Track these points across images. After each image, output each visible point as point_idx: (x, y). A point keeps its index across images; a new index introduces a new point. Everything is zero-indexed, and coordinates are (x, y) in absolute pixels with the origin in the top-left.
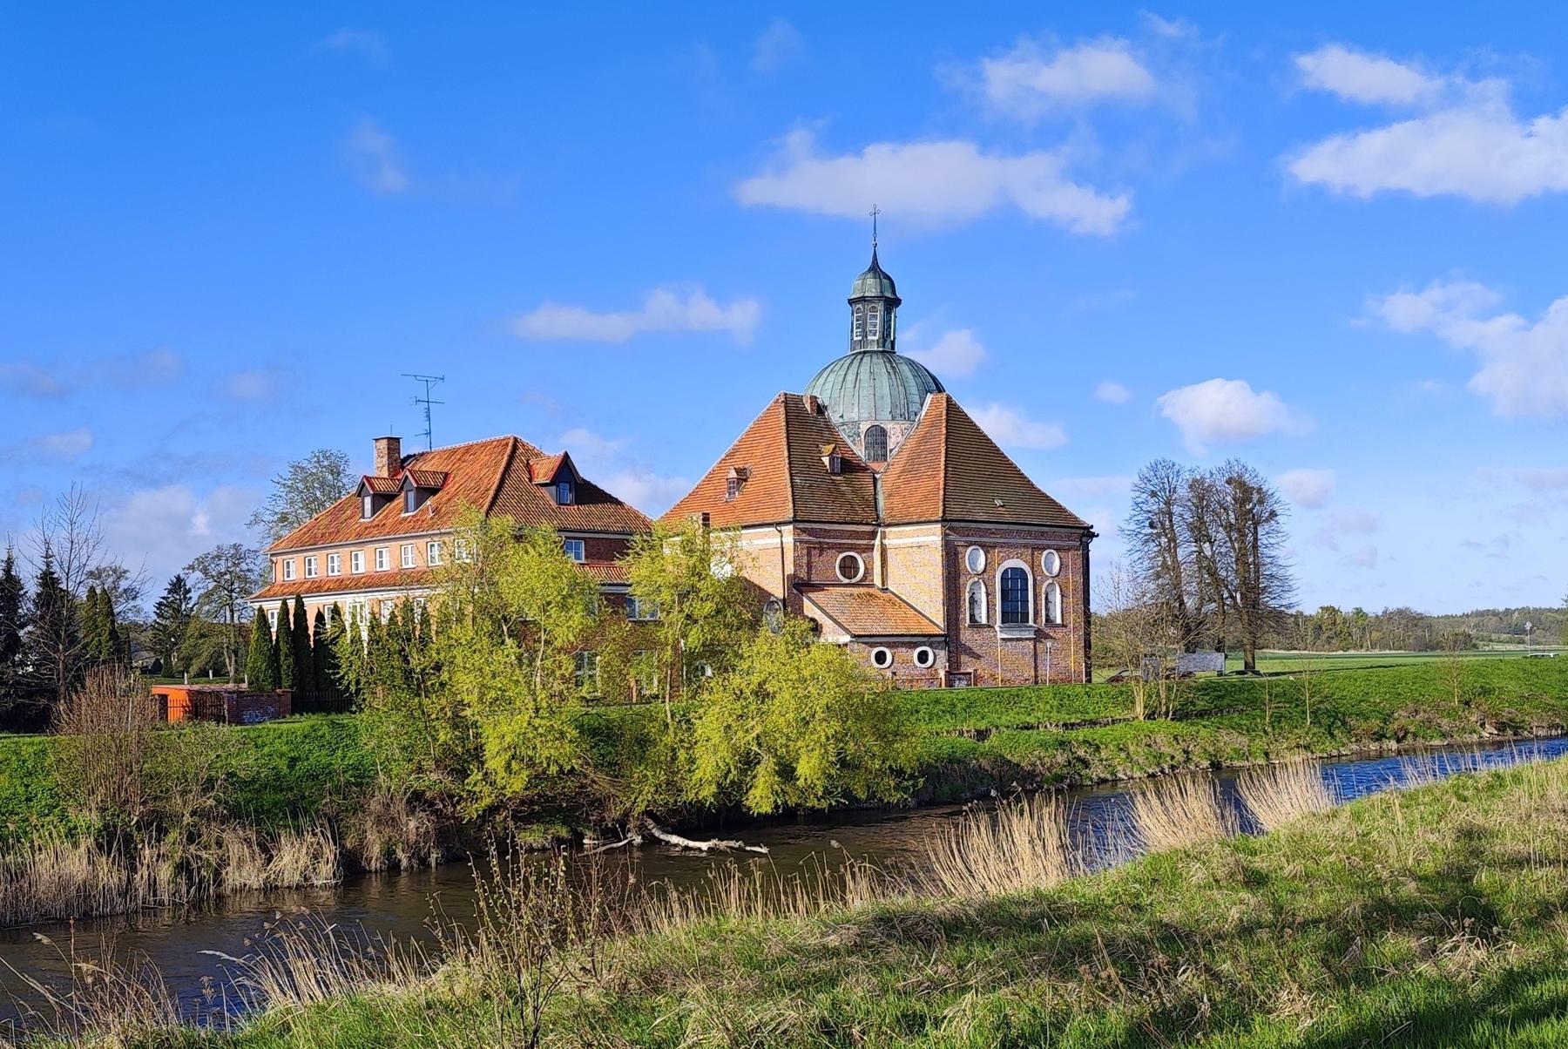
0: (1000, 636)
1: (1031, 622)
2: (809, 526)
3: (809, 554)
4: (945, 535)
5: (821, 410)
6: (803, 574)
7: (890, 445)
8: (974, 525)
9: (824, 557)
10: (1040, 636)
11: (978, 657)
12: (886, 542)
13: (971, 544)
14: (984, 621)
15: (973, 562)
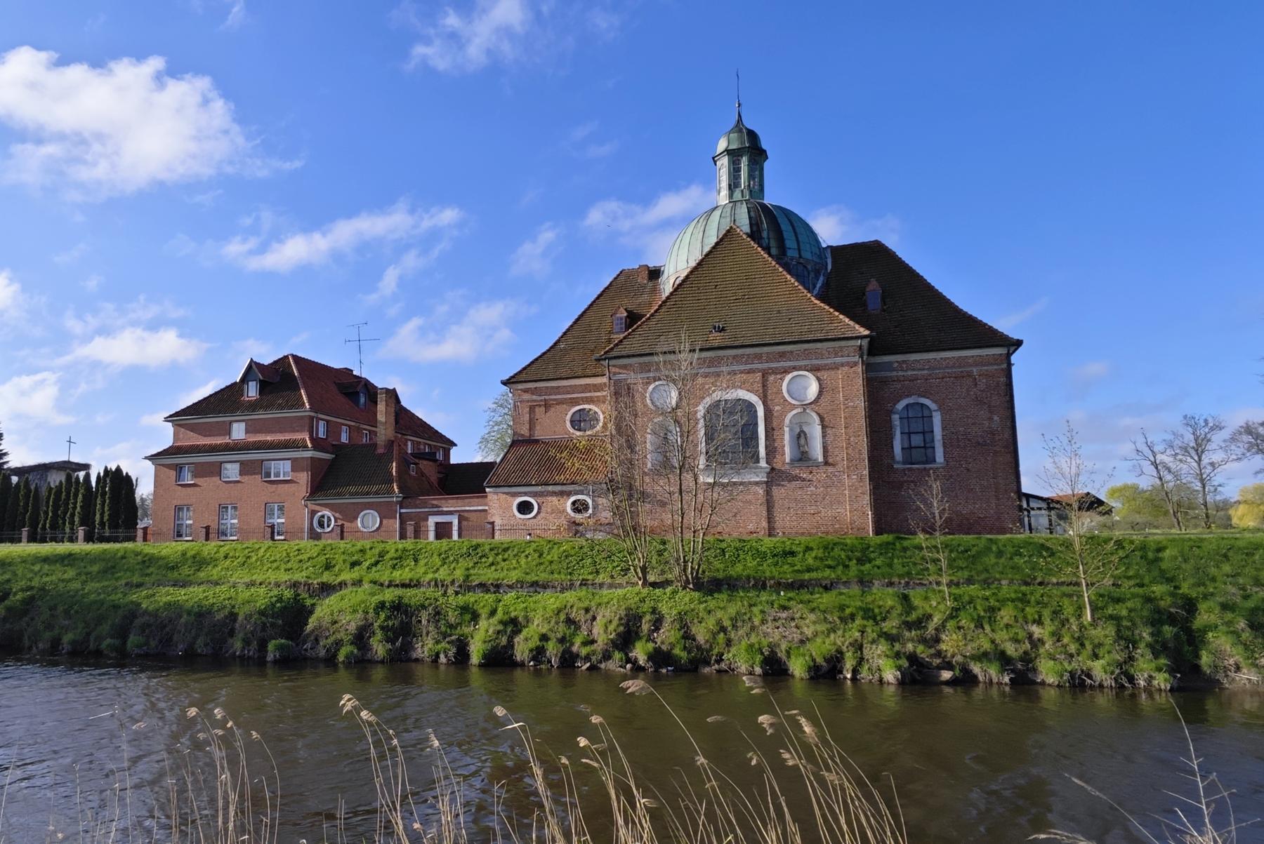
3: (532, 409)
6: (525, 431)
14: (821, 459)
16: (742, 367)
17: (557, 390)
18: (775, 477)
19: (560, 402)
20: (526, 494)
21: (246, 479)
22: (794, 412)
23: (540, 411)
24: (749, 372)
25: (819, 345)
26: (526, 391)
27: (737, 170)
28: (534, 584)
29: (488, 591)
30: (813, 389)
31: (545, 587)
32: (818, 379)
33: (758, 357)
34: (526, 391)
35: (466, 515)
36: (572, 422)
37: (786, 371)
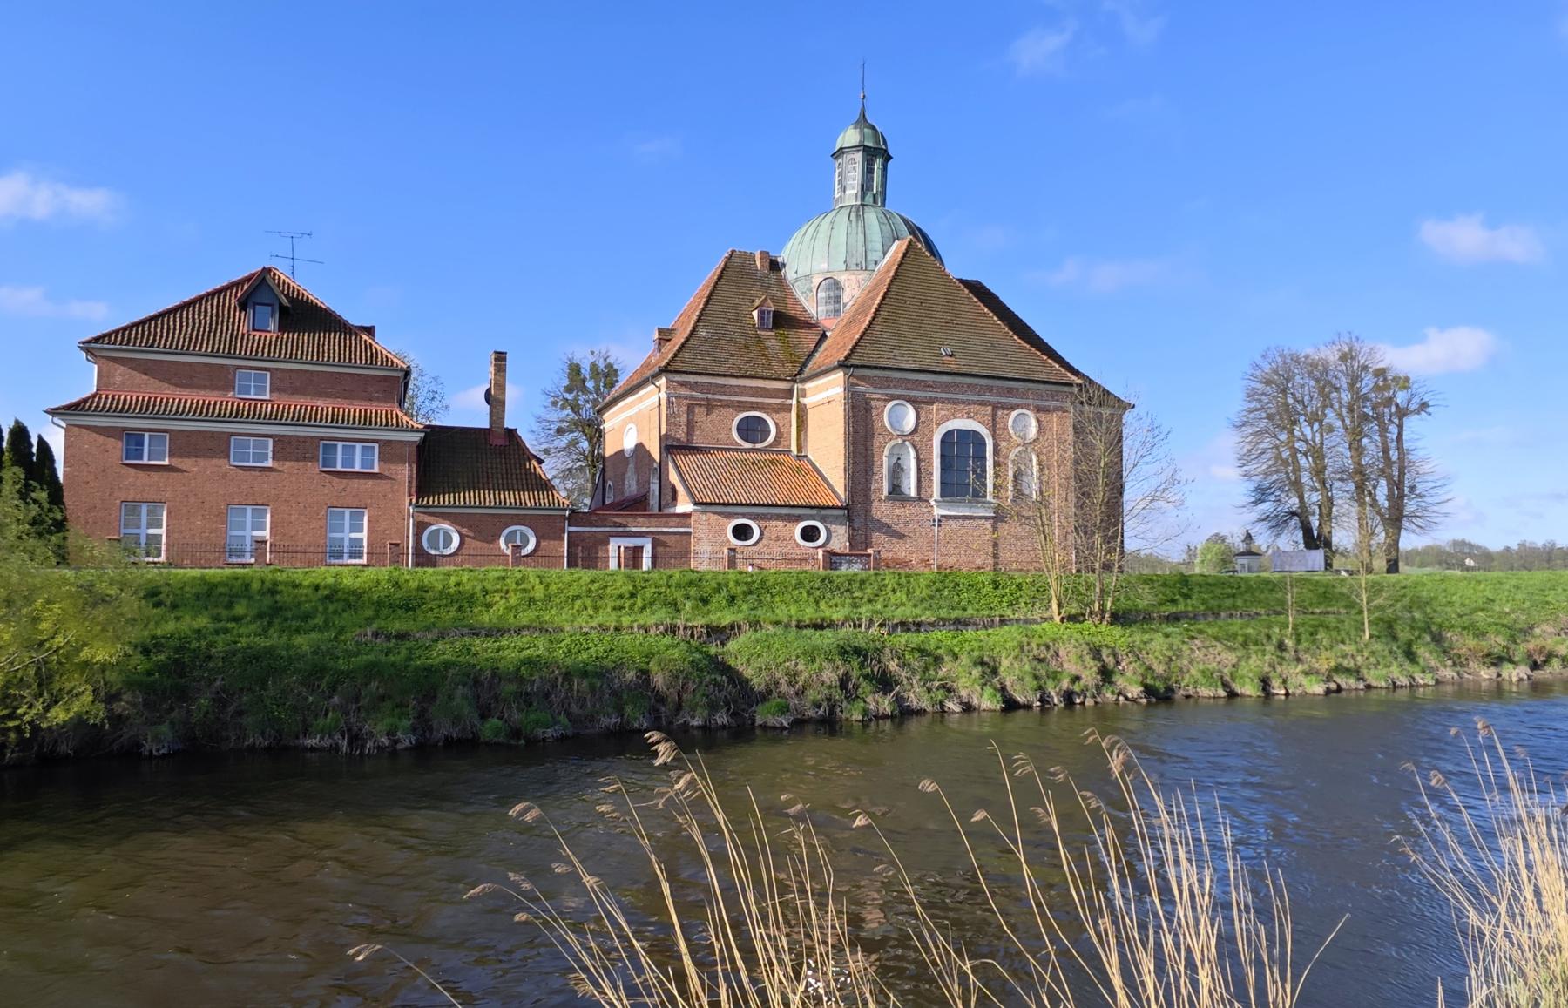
0: (938, 512)
1: (989, 498)
2: (692, 378)
3: (690, 408)
4: (849, 387)
5: (775, 266)
6: (681, 434)
7: (845, 299)
8: (897, 375)
9: (714, 415)
10: (998, 518)
11: (901, 536)
12: (804, 401)
13: (893, 398)
14: (913, 493)
15: (896, 420)
16: (976, 398)
17: (722, 389)
18: (998, 518)
19: (727, 405)
20: (744, 515)
21: (287, 466)
22: (893, 442)
23: (700, 412)
24: (982, 403)
25: (1041, 386)
26: (683, 384)
27: (870, 171)
28: (957, 621)
29: (908, 630)
30: (1033, 431)
31: (966, 624)
32: (1038, 420)
33: (990, 389)
34: (683, 384)
35: (662, 538)
36: (738, 429)
37: (1013, 408)
